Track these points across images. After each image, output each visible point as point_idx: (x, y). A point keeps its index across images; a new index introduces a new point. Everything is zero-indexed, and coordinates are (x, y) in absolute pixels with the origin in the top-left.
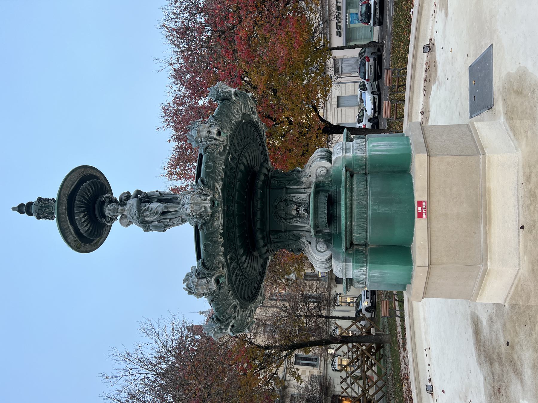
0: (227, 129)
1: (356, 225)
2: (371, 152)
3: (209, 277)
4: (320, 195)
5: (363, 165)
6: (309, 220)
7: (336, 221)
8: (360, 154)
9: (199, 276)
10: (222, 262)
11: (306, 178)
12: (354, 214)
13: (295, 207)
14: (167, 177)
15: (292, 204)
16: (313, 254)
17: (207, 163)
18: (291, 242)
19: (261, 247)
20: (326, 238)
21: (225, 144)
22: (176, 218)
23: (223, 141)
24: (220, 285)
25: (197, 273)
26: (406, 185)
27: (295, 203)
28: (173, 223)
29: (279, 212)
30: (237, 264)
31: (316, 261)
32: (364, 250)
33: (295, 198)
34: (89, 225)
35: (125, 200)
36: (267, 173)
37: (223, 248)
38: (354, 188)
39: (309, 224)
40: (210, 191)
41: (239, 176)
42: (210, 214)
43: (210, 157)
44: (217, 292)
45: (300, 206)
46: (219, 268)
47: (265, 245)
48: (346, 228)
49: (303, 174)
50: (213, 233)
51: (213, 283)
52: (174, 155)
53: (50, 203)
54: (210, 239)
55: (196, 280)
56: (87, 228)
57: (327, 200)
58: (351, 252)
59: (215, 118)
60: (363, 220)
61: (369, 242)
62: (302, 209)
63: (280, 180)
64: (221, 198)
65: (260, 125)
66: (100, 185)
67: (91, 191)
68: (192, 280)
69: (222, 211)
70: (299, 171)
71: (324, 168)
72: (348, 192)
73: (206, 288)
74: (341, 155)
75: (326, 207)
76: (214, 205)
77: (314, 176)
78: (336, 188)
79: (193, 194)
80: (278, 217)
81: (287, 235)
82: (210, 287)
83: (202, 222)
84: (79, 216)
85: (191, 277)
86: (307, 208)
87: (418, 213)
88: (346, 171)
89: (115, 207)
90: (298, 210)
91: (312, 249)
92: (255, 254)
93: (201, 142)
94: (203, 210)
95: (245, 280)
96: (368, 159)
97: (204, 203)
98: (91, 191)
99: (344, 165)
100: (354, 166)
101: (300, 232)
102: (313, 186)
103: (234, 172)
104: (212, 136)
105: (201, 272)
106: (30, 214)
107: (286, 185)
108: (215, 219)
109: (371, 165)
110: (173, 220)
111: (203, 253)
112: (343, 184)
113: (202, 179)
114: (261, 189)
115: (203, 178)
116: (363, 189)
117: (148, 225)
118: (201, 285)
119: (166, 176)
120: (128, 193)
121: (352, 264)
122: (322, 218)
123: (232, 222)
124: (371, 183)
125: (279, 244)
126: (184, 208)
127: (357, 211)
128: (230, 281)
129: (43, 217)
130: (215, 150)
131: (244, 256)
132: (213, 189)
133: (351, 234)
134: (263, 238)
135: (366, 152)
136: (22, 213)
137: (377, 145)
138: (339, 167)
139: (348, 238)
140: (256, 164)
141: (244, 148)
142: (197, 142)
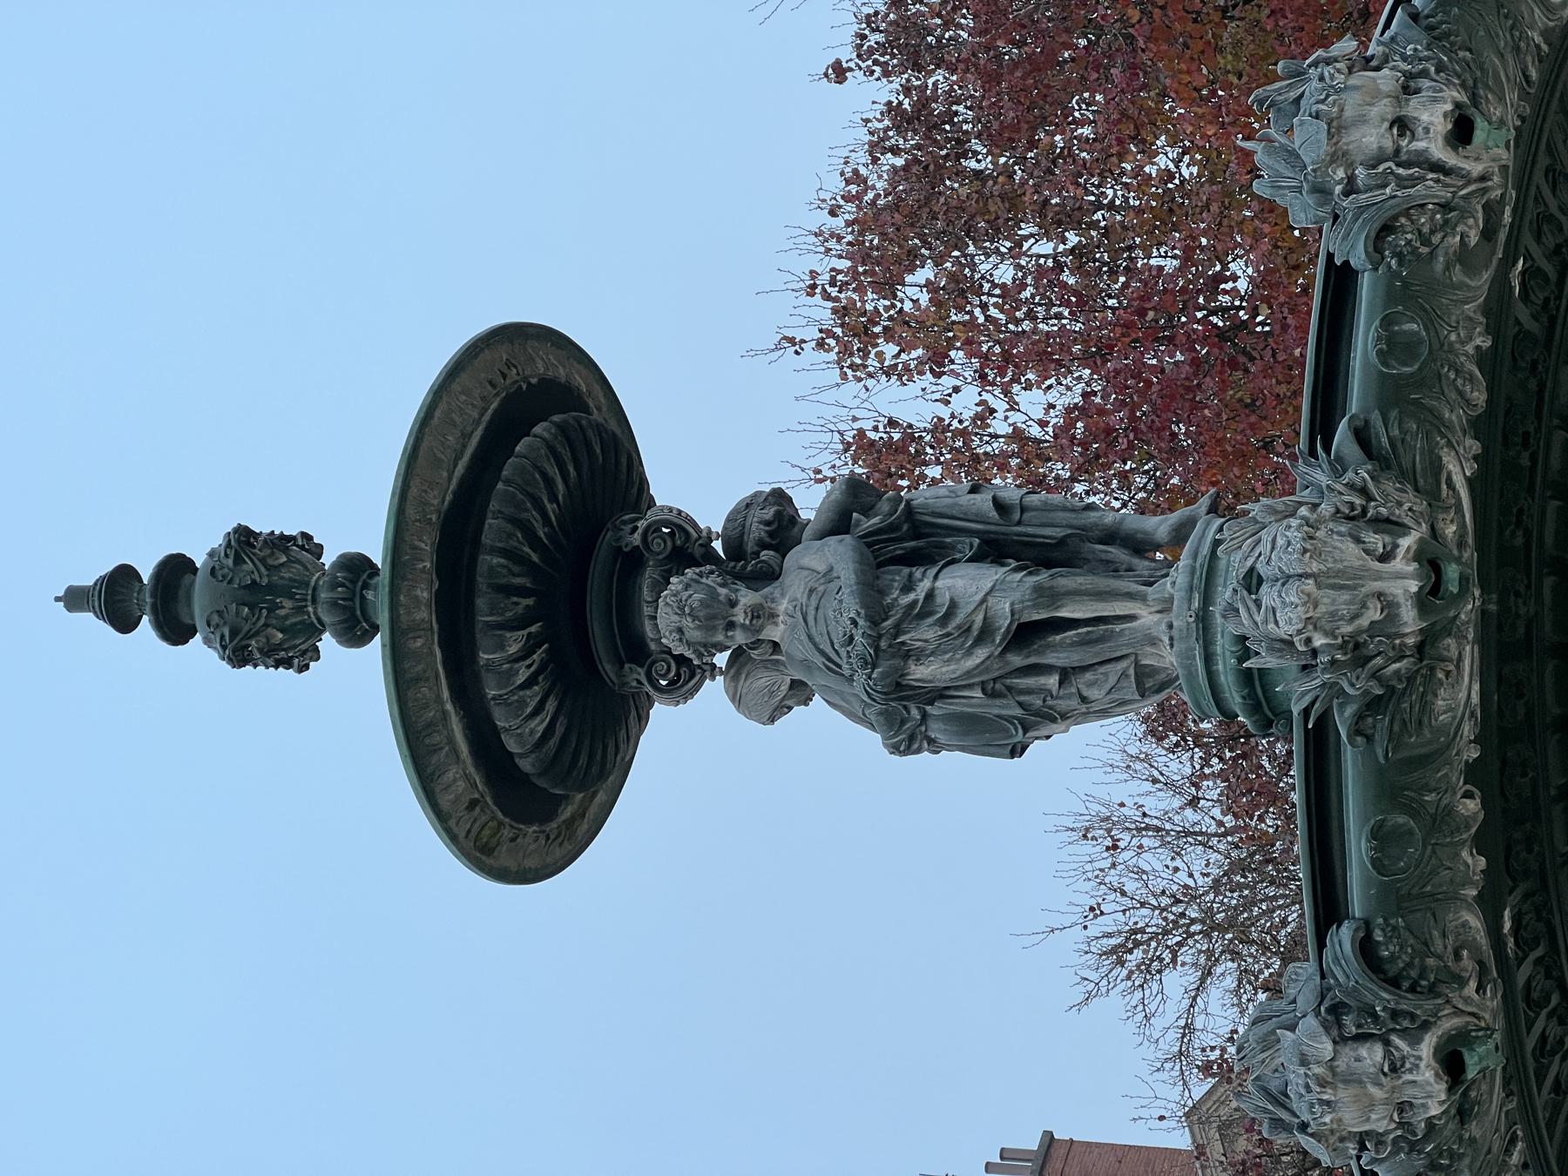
0: (1501, 99)
3: (1403, 1033)
9: (1340, 1026)
14: (833, 356)
17: (1387, 322)
22: (1102, 669)
23: (1483, 178)
24: (1465, 1094)
25: (1327, 1003)
28: (1084, 699)
30: (1548, 976)
34: (551, 706)
35: (763, 546)
37: (1482, 862)
40: (1411, 500)
42: (1411, 641)
43: (1406, 285)
46: (1462, 982)
51: (1429, 1075)
52: (857, 178)
53: (298, 561)
54: (1412, 800)
55: (1326, 1047)
56: (539, 725)
64: (1470, 541)
66: (602, 449)
67: (561, 486)
68: (1297, 1043)
69: (1475, 626)
73: (1386, 1102)
82: (1408, 1094)
83: (1366, 693)
84: (502, 647)
89: (713, 594)
93: (1346, 193)
94: (1377, 616)
97: (1379, 577)
98: (561, 486)
103: (1534, 363)
105: (1352, 1003)
106: (175, 631)
108: (1441, 675)
110: (1081, 682)
111: (1367, 882)
113: (1360, 423)
115: (1366, 422)
117: (915, 713)
118: (1351, 1079)
119: (821, 344)
120: (780, 498)
123: (1521, 696)
126: (1258, 603)
128: (1514, 1079)
129: (260, 650)
130: (1436, 239)
132: (1429, 484)
136: (124, 624)
142: (1321, 191)
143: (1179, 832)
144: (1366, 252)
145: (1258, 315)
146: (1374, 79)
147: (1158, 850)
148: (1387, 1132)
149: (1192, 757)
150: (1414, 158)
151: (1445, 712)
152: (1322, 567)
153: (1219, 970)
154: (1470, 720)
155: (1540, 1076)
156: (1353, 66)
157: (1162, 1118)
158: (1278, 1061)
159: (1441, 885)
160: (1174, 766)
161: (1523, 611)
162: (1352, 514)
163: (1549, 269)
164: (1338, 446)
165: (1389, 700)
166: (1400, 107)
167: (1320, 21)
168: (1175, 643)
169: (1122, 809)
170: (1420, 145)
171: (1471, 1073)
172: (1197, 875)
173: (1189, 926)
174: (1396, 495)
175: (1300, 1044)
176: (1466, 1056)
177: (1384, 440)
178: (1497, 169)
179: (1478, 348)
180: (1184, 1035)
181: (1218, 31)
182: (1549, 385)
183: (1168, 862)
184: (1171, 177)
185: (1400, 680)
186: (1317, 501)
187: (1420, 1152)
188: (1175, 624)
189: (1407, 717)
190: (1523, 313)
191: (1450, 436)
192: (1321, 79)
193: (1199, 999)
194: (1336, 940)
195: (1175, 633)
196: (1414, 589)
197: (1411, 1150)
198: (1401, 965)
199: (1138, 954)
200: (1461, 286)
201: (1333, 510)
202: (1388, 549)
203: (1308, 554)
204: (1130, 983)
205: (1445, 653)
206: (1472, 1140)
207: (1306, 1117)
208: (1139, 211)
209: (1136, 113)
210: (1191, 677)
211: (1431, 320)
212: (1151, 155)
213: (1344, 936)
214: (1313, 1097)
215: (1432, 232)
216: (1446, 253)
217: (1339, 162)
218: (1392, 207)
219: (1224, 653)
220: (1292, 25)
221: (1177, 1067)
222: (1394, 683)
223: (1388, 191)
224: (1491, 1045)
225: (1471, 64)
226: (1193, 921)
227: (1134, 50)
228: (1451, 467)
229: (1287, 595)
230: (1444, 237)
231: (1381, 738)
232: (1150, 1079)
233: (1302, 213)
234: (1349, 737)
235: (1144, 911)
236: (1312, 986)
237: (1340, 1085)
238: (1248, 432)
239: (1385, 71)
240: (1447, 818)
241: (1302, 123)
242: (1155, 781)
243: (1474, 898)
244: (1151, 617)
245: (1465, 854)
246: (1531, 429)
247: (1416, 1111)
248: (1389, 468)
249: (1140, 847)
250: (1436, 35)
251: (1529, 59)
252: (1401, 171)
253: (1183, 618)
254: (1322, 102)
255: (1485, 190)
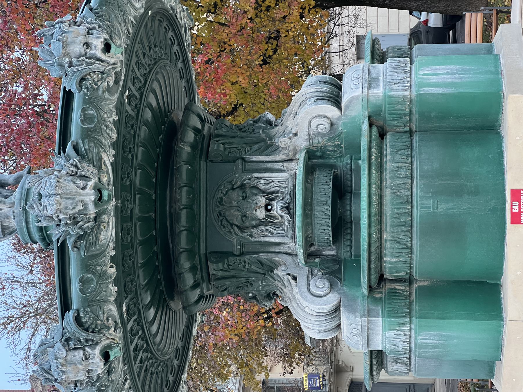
0: (120, 38)
1: (389, 238)
2: (421, 87)
4: (317, 176)
5: (404, 114)
6: (294, 229)
7: (349, 232)
8: (398, 93)
9: (69, 345)
10: (113, 317)
11: (286, 140)
12: (386, 215)
13: (262, 201)
15: (256, 195)
16: (301, 300)
17: (84, 110)
18: (253, 278)
19: (187, 288)
20: (327, 268)
21: (119, 69)
23: (114, 64)
24: (110, 365)
25: (64, 338)
26: (490, 156)
27: (263, 192)
29: (227, 213)
30: (138, 325)
31: (308, 317)
32: (407, 291)
33: (264, 181)
36: (199, 126)
37: (116, 289)
38: (386, 162)
39: (294, 238)
40: (92, 169)
41: (142, 135)
43: (90, 98)
44: (104, 379)
45: (273, 199)
46: (109, 328)
47: (196, 286)
48: (369, 245)
49: (279, 129)
50: (97, 256)
51: (98, 360)
54: (93, 269)
55: (64, 353)
57: (331, 186)
58: (379, 296)
59: (96, 13)
60: (403, 228)
61: (416, 273)
62: (277, 207)
63: (230, 143)
64: (112, 183)
65: (178, 14)
69: (114, 211)
70: (269, 122)
71: (324, 119)
72: (374, 172)
74: (359, 92)
75: (330, 202)
76: (100, 199)
77: (303, 135)
78: (349, 161)
79: (59, 175)
80: (225, 223)
81: (245, 262)
83: (78, 234)
85: (52, 347)
86: (289, 203)
87: (512, 214)
88: (371, 125)
90: (269, 207)
91: (300, 291)
92: (172, 304)
93: (69, 67)
94: (81, 208)
95: (151, 361)
96: (414, 102)
99: (366, 112)
100: (387, 115)
101: (273, 255)
102: (301, 157)
103: (133, 125)
104: (93, 55)
107: (243, 153)
109: (421, 115)
112: (364, 154)
113: (75, 144)
114: (188, 163)
115: (77, 143)
116: (404, 165)
118: (72, 363)
121: (380, 319)
122: (322, 225)
123: (129, 234)
124: (420, 153)
125: (227, 283)
126: (41, 204)
127: (392, 211)
128: (127, 360)
130: (99, 83)
131: (152, 308)
133: (380, 258)
134: (193, 269)
135: (410, 87)
137: (434, 72)
138: (354, 117)
139: (373, 266)
140: (173, 105)
141: (150, 71)
143: (26, 283)
144: (77, 87)
145: (50, 107)
146: (78, 29)
147: (19, 289)
148: (84, 380)
149: (30, 257)
150: (91, 56)
151: (104, 240)
152: (62, 192)
153: (39, 329)
154: (112, 242)
155: (135, 358)
156: (71, 24)
157: (19, 380)
158: (48, 359)
159: (102, 297)
160: (24, 260)
161: (129, 206)
162: (73, 174)
163: (137, 95)
164: (68, 152)
165: (85, 236)
166: (86, 39)
167: (68, 10)
168: (15, 218)
169: (6, 275)
170: (93, 52)
171: (112, 358)
172: (32, 297)
173: (29, 314)
174: (87, 167)
175: (55, 352)
176: (110, 353)
177: (83, 149)
178: (119, 61)
179: (114, 120)
180: (27, 352)
181: (35, 11)
182: (137, 132)
183: (22, 293)
184: (19, 59)
185: (89, 229)
186: (61, 169)
187: (95, 386)
188: (15, 211)
189: (91, 241)
190: (128, 108)
191: (104, 148)
192: (60, 28)
193: (32, 339)
194: (67, 317)
195: (15, 214)
196: (93, 199)
197: (92, 385)
198: (89, 324)
199: (12, 325)
200: (108, 99)
201: (66, 173)
202: (85, 185)
203: (57, 187)
204: (9, 335)
205: (103, 220)
206: (112, 381)
207: (57, 377)
208: (9, 71)
209: (7, 37)
210: (21, 229)
211: (98, 110)
212: (13, 52)
213: (70, 315)
214: (59, 370)
215: (98, 81)
216: (103, 88)
217: (66, 56)
218: (84, 72)
219: (32, 221)
220: (59, 10)
221: (25, 363)
222: (87, 230)
223: (83, 66)
224: (118, 349)
225: (110, 26)
226: (31, 313)
227: (6, 16)
228: (105, 159)
229: (50, 201)
230: (102, 83)
231: (83, 249)
232: (15, 368)
233: (55, 73)
234: (72, 248)
235: (14, 310)
236: (60, 333)
237: (68, 365)
238: (47, 147)
239: (81, 27)
240: (104, 275)
241: (54, 42)
242: (18, 265)
243: (114, 301)
244: (7, 209)
245: (110, 286)
246: (132, 147)
247: (93, 372)
248: (84, 159)
249: (13, 288)
250: (98, 16)
251: (129, 26)
252: (87, 60)
253: (18, 210)
254: (61, 35)
255: (115, 68)
